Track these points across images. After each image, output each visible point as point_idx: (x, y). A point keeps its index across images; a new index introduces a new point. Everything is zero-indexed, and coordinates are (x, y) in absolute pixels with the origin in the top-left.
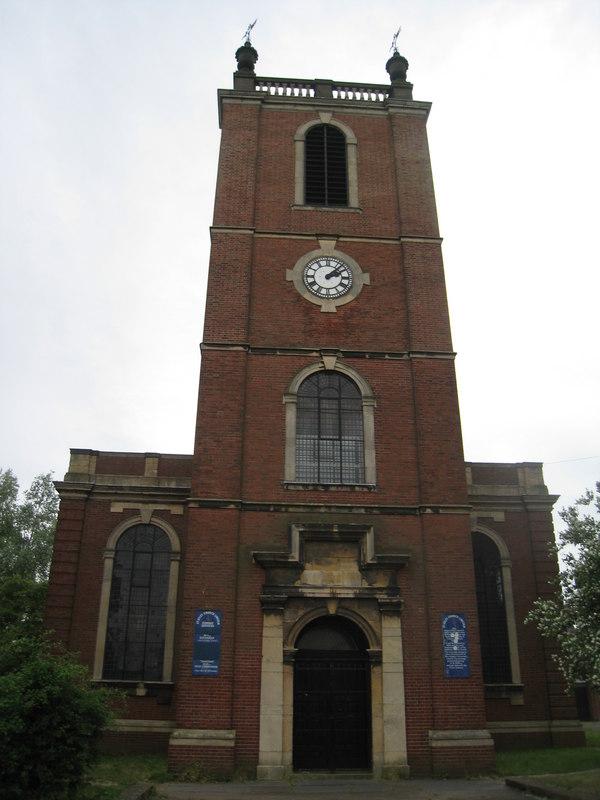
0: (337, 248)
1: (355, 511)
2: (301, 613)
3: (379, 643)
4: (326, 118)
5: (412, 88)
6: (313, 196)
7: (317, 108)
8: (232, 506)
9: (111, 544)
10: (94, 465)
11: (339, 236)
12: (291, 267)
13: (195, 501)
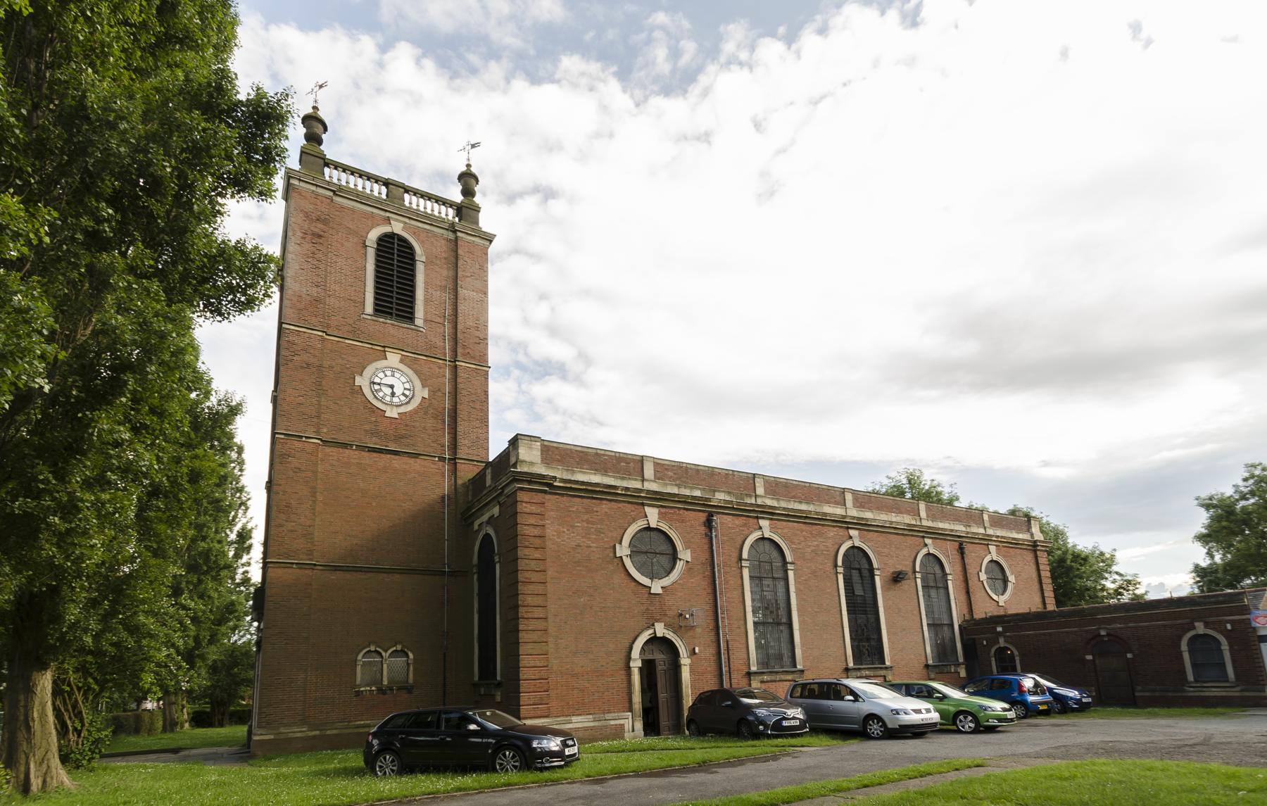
4: (397, 228)
5: (479, 211)
6: (381, 308)
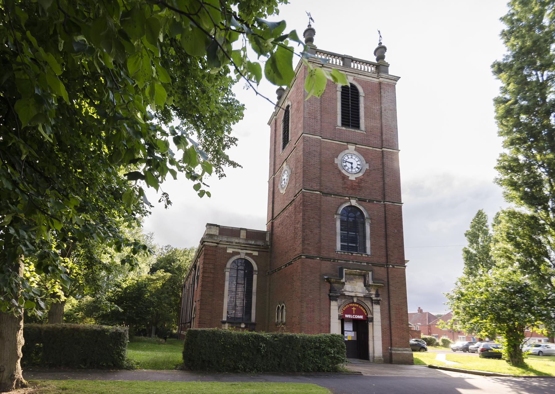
0: (355, 150)
1: (363, 264)
2: (343, 301)
3: (372, 314)
6: (345, 123)
7: (347, 73)
8: (318, 258)
9: (228, 265)
10: (218, 231)
11: (356, 144)
12: (337, 157)
13: (304, 256)
